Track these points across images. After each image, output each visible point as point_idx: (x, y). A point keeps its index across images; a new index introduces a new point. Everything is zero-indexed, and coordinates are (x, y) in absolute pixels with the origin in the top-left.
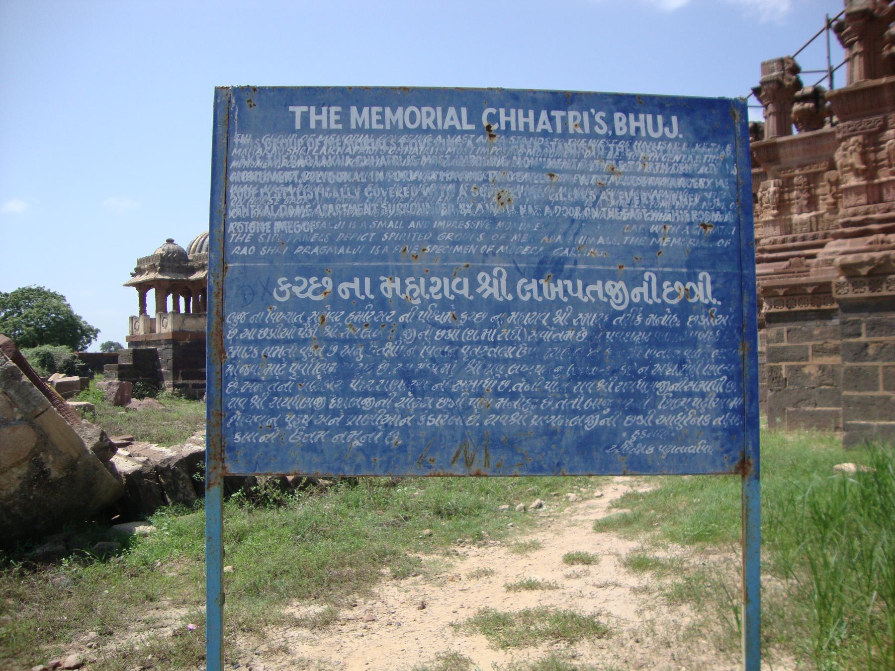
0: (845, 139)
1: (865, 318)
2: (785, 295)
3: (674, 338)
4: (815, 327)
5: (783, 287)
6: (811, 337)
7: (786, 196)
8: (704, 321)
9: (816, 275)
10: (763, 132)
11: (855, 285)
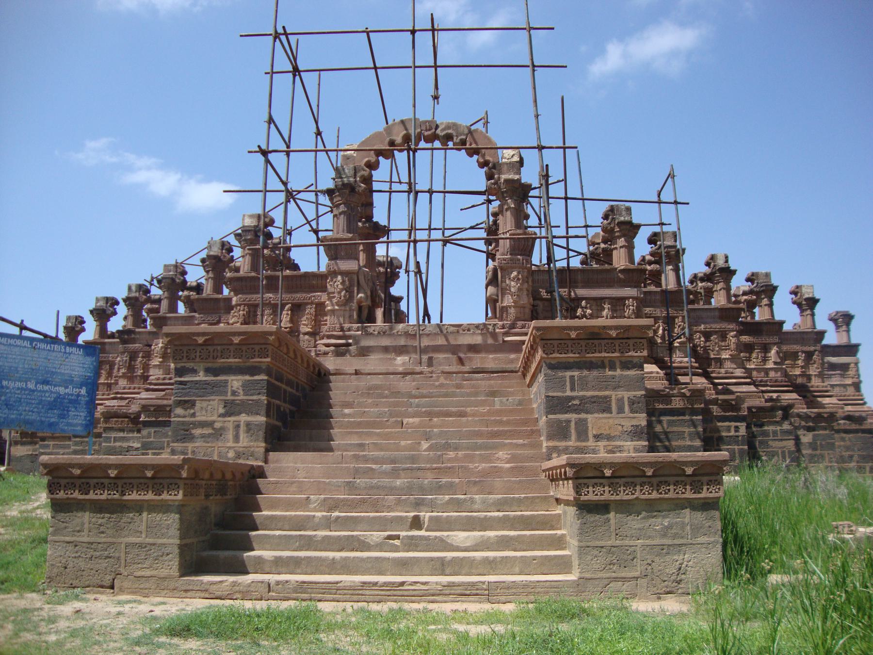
3: (75, 402)
5: (153, 406)
6: (167, 436)
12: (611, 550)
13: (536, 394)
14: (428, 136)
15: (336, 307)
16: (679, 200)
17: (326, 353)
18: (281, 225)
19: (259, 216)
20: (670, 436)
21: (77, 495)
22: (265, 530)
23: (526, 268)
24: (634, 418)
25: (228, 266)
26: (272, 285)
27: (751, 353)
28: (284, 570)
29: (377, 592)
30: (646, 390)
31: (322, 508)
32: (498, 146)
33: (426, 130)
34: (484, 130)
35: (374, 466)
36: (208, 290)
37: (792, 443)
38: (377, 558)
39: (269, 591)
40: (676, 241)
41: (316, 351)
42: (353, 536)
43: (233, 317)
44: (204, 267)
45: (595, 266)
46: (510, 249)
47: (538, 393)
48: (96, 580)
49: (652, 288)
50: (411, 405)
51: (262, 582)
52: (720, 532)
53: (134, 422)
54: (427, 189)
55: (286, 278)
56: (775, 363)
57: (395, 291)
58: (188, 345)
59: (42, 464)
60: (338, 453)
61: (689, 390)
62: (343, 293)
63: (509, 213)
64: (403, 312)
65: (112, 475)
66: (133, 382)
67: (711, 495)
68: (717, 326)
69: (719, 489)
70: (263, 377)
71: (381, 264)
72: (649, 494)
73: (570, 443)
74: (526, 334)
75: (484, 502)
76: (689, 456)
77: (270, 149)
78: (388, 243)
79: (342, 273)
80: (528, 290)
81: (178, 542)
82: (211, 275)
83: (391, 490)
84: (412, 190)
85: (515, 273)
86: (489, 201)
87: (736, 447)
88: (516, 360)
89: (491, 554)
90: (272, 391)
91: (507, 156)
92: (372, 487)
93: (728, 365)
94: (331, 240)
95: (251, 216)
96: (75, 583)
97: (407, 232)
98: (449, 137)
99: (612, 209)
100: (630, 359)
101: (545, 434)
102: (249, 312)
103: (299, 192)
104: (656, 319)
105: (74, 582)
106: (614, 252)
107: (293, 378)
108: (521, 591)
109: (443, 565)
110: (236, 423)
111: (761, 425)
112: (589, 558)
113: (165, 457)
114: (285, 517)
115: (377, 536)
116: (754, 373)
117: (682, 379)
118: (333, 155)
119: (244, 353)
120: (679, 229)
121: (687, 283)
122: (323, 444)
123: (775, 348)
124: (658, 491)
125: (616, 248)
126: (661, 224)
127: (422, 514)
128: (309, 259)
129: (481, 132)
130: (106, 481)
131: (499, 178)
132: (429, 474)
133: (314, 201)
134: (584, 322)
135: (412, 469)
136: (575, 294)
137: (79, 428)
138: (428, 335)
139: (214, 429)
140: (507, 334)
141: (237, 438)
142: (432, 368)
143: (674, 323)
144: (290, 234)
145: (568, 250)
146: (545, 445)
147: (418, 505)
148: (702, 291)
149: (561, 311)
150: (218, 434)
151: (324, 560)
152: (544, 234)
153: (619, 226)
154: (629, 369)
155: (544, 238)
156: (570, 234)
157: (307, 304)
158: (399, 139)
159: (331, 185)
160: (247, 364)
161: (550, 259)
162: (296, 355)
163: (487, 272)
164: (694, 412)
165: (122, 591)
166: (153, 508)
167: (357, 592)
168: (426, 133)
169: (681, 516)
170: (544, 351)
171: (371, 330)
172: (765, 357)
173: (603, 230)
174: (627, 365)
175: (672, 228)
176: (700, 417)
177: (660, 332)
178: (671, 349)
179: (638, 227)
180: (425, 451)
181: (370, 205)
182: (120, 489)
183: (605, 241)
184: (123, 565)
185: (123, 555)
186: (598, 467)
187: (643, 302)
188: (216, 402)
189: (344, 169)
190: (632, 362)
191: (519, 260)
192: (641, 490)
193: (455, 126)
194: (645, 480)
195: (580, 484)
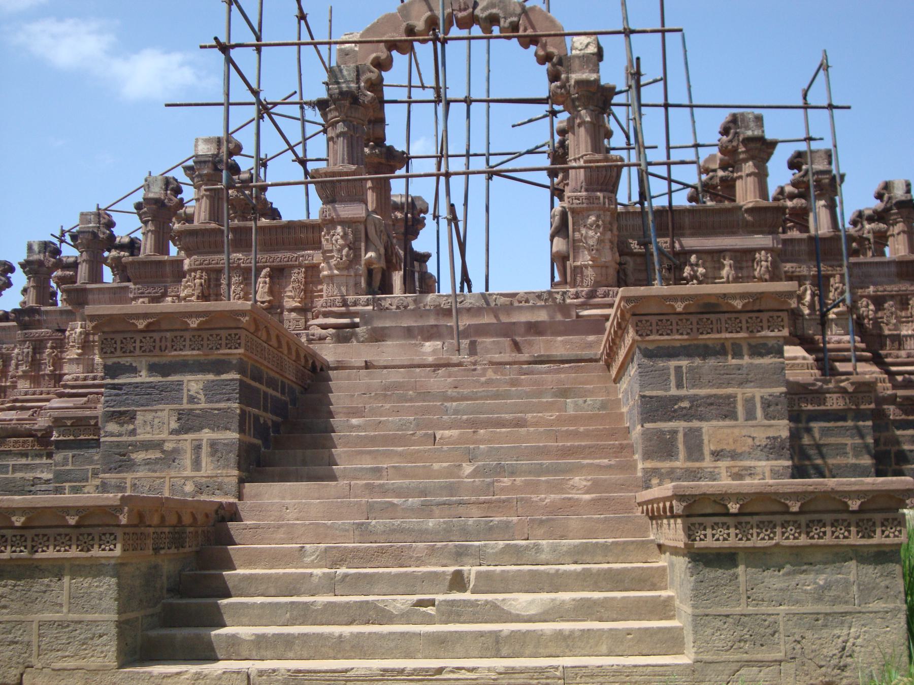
2: (72, 425)
5: (71, 418)
6: (91, 462)
10: (139, 249)
13: (626, 392)
15: (336, 272)
16: (835, 103)
17: (322, 339)
18: (253, 153)
19: (219, 141)
20: (824, 450)
22: (241, 596)
23: (608, 210)
25: (175, 214)
26: (241, 240)
28: (269, 653)
30: (788, 384)
31: (323, 563)
32: (566, 31)
33: (460, 10)
34: (544, 7)
35: (395, 501)
36: (147, 249)
38: (403, 634)
40: (830, 163)
41: (307, 335)
42: (367, 602)
43: (186, 287)
44: (140, 215)
45: (709, 203)
46: (584, 178)
47: (628, 390)
49: (795, 234)
50: (446, 412)
51: (238, 673)
52: (902, 596)
53: (43, 442)
54: (462, 97)
55: (261, 230)
57: (420, 245)
60: (343, 483)
61: (852, 384)
62: (345, 252)
63: (582, 131)
64: (431, 276)
65: (17, 524)
66: (39, 385)
67: (888, 541)
68: (893, 288)
69: (900, 532)
71: (398, 207)
72: (795, 538)
73: (677, 464)
74: (611, 306)
75: (554, 549)
76: (855, 484)
77: (233, 42)
78: (407, 177)
79: (344, 223)
80: (611, 242)
81: (115, 617)
82: (151, 227)
83: (422, 535)
84: (440, 98)
85: (592, 219)
86: (554, 113)
88: (598, 344)
89: (567, 626)
90: (247, 395)
91: (579, 45)
92: (393, 531)
94: (326, 174)
97: (434, 160)
98: (493, 20)
99: (734, 120)
100: (762, 341)
101: (640, 450)
102: (208, 281)
103: (275, 104)
104: (800, 280)
106: (739, 184)
107: (277, 376)
108: (612, 679)
109: (497, 642)
110: (197, 443)
112: (709, 631)
113: (90, 495)
114: (269, 577)
115: (402, 601)
117: (841, 367)
118: (324, 49)
119: (205, 342)
120: (835, 146)
121: (847, 225)
122: (320, 470)
124: (808, 534)
125: (740, 177)
126: (809, 139)
127: (465, 568)
128: (294, 204)
129: (541, 11)
130: (8, 533)
131: (568, 79)
132: (475, 511)
133: (299, 116)
134: (692, 288)
135: (450, 504)
136: (681, 245)
138: (469, 310)
139: (163, 452)
140: (584, 306)
141: (197, 464)
142: (476, 357)
143: (828, 285)
144: (265, 165)
145: (670, 180)
146: (640, 466)
147: (460, 555)
148: (871, 236)
149: (660, 272)
150: (170, 458)
151: (329, 637)
152: (634, 160)
153: (746, 144)
154: (762, 355)
155: (634, 165)
156: (673, 159)
157: (293, 267)
158: (420, 25)
159: (324, 95)
160: (210, 357)
161: (644, 195)
162: (279, 341)
163: (553, 217)
164: (860, 415)
166: (78, 569)
168: (460, 15)
169: (844, 570)
170: (637, 332)
171: (386, 304)
173: (721, 151)
174: (758, 350)
175: (827, 145)
176: (870, 423)
177: (808, 298)
178: (823, 323)
179: (773, 144)
180: (468, 477)
181: (380, 121)
182: (29, 544)
183: (724, 167)
184: (35, 653)
185: (35, 639)
186: (720, 499)
187: (780, 255)
188: (166, 413)
189: (341, 71)
190: (765, 344)
191: (598, 198)
192: (783, 533)
194: (788, 517)
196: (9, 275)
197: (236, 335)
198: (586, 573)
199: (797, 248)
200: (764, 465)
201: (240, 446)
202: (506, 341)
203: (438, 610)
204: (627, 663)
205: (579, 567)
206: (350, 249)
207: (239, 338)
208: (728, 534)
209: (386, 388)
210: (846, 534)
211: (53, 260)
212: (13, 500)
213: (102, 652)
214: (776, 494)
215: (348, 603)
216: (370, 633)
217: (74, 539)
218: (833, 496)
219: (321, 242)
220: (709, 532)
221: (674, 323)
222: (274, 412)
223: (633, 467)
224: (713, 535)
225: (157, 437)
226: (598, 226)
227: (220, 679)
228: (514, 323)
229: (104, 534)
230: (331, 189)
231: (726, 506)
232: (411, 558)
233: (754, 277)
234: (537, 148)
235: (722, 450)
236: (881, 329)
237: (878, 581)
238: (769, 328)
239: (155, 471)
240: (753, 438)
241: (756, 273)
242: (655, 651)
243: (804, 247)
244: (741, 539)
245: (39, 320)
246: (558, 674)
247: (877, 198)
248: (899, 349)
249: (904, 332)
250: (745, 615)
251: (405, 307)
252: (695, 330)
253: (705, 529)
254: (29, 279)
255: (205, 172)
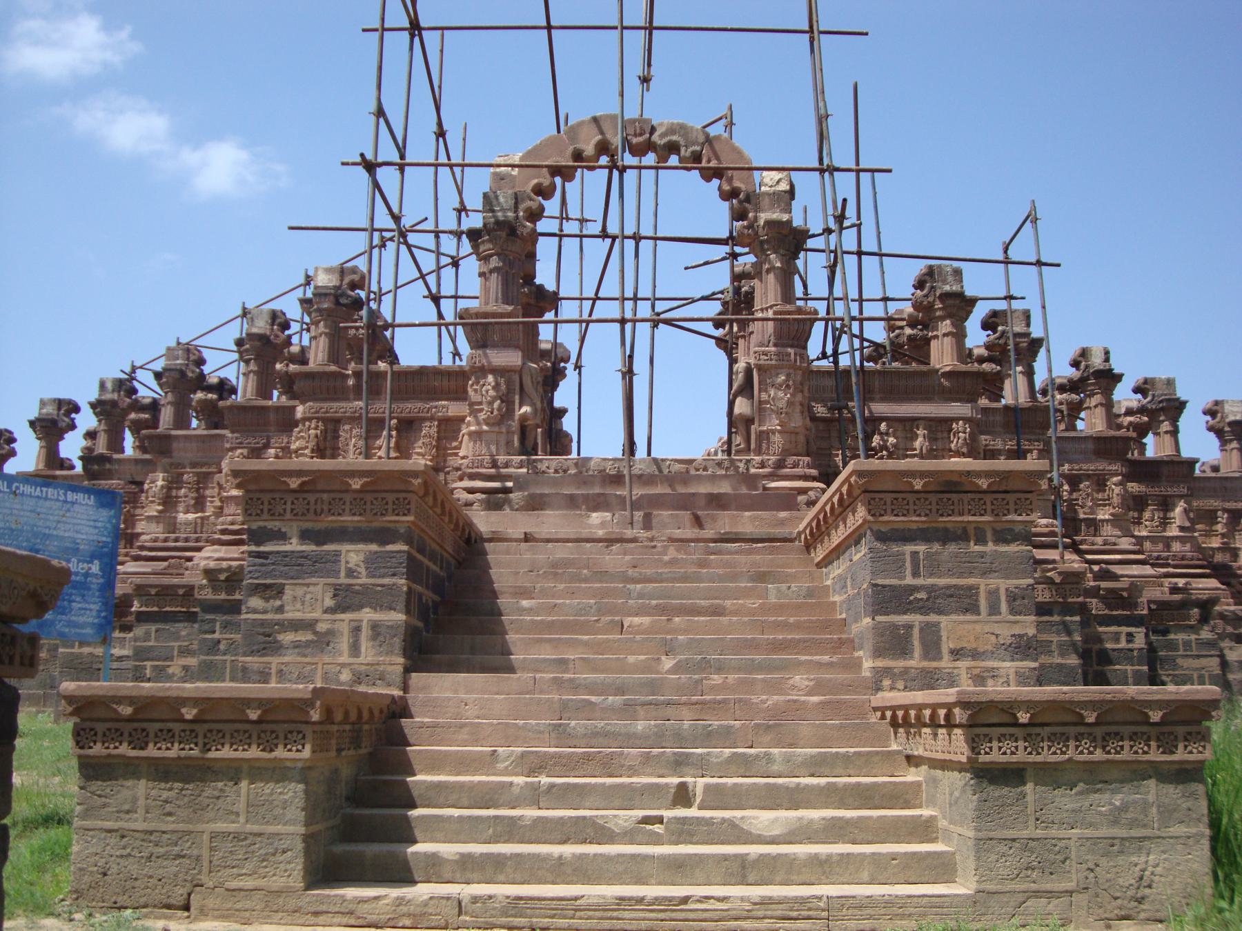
0: (232, 449)
1: (220, 618)
2: (156, 595)
4: (183, 629)
5: (156, 586)
7: (174, 493)
8: (94, 580)
9: (193, 577)
11: (215, 590)
12: (1027, 845)
14: (638, 144)
15: (485, 428)
16: (1043, 260)
17: (469, 504)
21: (124, 749)
23: (800, 368)
24: (1016, 622)
27: (1141, 511)
28: (475, 876)
29: (642, 915)
31: (518, 770)
32: (754, 165)
33: (635, 135)
35: (593, 699)
36: (245, 391)
37: (1216, 661)
38: (634, 857)
39: (460, 914)
40: (1028, 325)
43: (298, 439)
48: (158, 895)
51: (448, 898)
56: (1182, 528)
58: (271, 491)
59: (65, 697)
60: (523, 676)
62: (496, 405)
63: (771, 277)
65: (188, 717)
67: (1191, 757)
69: (1204, 747)
70: (401, 547)
72: (1090, 753)
75: (788, 759)
76: (1157, 692)
77: (380, 160)
78: (556, 323)
79: (496, 371)
80: (801, 404)
81: (302, 830)
82: (253, 366)
83: (630, 739)
86: (734, 256)
87: (1129, 668)
90: (414, 571)
91: (769, 181)
92: (596, 734)
93: (1108, 530)
94: (477, 315)
95: (329, 270)
96: (122, 900)
98: (673, 148)
99: (930, 272)
100: (1008, 526)
102: (325, 432)
105: (120, 899)
106: (933, 343)
107: (437, 548)
109: (743, 867)
110: (355, 624)
111: (1165, 632)
112: (993, 857)
114: (461, 785)
115: (626, 817)
116: (1147, 545)
119: (368, 507)
122: (497, 660)
123: (1182, 503)
124: (1104, 748)
125: (936, 337)
126: (1010, 298)
130: (177, 727)
131: (756, 219)
132: (686, 712)
133: (433, 247)
137: (88, 631)
139: (315, 633)
140: (773, 476)
141: (355, 649)
147: (679, 764)
150: (324, 641)
153: (941, 299)
158: (589, 150)
160: (376, 525)
164: (1067, 609)
165: (204, 914)
166: (258, 772)
167: (609, 914)
168: (635, 140)
169: (1142, 789)
172: (1165, 518)
173: (913, 306)
176: (1077, 618)
179: (972, 302)
180: (669, 672)
181: (532, 256)
182: (201, 740)
184: (205, 870)
185: (206, 853)
187: (978, 426)
188: (320, 587)
189: (497, 197)
192: (1077, 747)
193: (682, 129)
194: (1082, 729)
195: (977, 736)
196: (73, 415)
197: (405, 499)
198: (831, 788)
199: (991, 418)
200: (1008, 666)
201: (406, 630)
202: (686, 515)
203: (666, 828)
204: (899, 893)
205: (823, 781)
206: (502, 401)
207: (409, 503)
208: (1016, 748)
209: (555, 565)
210: (1146, 748)
211: (128, 400)
212: (184, 689)
213: (286, 871)
214: (1071, 702)
215: (561, 818)
216: (595, 855)
217: (255, 737)
218: (1133, 705)
219: (467, 392)
220: (995, 744)
221: (911, 503)
222: (435, 591)
223: (856, 665)
224: (1000, 748)
225: (308, 616)
226: (788, 386)
227: (426, 905)
228: (694, 494)
229: (291, 732)
230: (481, 331)
231: (1014, 716)
232: (622, 766)
233: (950, 450)
234: (714, 294)
235: (962, 649)
236: (1076, 511)
237: (1179, 802)
238: (1016, 511)
239: (305, 656)
240: (997, 636)
241: (953, 446)
242: (923, 880)
243: (999, 418)
244: (1030, 753)
245: (109, 470)
246: (822, 904)
247: (1072, 366)
248: (1095, 535)
249: (1100, 517)
250: (1033, 840)
251: (565, 471)
252: (934, 510)
253: (990, 742)
254: (100, 421)
255: (326, 306)
